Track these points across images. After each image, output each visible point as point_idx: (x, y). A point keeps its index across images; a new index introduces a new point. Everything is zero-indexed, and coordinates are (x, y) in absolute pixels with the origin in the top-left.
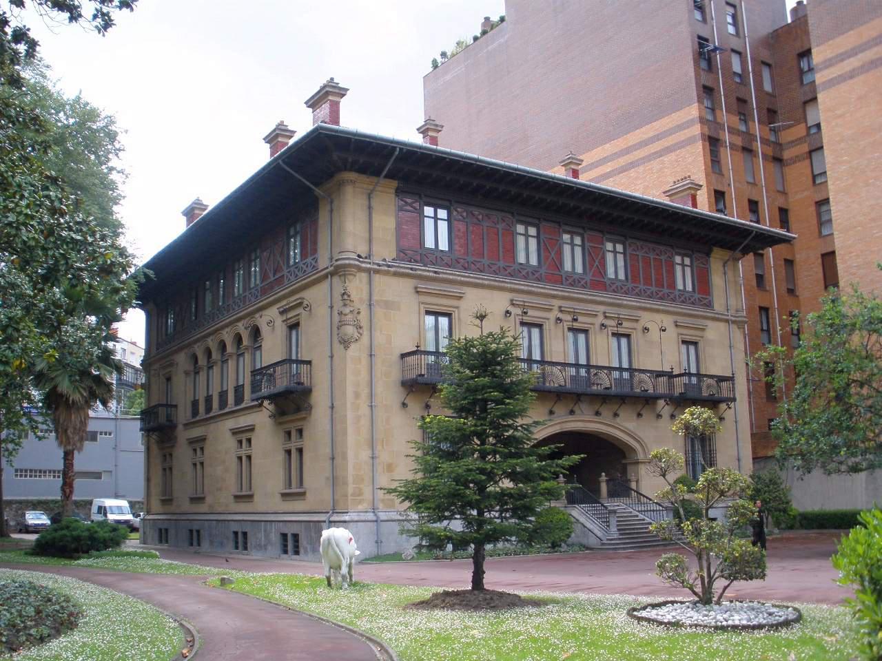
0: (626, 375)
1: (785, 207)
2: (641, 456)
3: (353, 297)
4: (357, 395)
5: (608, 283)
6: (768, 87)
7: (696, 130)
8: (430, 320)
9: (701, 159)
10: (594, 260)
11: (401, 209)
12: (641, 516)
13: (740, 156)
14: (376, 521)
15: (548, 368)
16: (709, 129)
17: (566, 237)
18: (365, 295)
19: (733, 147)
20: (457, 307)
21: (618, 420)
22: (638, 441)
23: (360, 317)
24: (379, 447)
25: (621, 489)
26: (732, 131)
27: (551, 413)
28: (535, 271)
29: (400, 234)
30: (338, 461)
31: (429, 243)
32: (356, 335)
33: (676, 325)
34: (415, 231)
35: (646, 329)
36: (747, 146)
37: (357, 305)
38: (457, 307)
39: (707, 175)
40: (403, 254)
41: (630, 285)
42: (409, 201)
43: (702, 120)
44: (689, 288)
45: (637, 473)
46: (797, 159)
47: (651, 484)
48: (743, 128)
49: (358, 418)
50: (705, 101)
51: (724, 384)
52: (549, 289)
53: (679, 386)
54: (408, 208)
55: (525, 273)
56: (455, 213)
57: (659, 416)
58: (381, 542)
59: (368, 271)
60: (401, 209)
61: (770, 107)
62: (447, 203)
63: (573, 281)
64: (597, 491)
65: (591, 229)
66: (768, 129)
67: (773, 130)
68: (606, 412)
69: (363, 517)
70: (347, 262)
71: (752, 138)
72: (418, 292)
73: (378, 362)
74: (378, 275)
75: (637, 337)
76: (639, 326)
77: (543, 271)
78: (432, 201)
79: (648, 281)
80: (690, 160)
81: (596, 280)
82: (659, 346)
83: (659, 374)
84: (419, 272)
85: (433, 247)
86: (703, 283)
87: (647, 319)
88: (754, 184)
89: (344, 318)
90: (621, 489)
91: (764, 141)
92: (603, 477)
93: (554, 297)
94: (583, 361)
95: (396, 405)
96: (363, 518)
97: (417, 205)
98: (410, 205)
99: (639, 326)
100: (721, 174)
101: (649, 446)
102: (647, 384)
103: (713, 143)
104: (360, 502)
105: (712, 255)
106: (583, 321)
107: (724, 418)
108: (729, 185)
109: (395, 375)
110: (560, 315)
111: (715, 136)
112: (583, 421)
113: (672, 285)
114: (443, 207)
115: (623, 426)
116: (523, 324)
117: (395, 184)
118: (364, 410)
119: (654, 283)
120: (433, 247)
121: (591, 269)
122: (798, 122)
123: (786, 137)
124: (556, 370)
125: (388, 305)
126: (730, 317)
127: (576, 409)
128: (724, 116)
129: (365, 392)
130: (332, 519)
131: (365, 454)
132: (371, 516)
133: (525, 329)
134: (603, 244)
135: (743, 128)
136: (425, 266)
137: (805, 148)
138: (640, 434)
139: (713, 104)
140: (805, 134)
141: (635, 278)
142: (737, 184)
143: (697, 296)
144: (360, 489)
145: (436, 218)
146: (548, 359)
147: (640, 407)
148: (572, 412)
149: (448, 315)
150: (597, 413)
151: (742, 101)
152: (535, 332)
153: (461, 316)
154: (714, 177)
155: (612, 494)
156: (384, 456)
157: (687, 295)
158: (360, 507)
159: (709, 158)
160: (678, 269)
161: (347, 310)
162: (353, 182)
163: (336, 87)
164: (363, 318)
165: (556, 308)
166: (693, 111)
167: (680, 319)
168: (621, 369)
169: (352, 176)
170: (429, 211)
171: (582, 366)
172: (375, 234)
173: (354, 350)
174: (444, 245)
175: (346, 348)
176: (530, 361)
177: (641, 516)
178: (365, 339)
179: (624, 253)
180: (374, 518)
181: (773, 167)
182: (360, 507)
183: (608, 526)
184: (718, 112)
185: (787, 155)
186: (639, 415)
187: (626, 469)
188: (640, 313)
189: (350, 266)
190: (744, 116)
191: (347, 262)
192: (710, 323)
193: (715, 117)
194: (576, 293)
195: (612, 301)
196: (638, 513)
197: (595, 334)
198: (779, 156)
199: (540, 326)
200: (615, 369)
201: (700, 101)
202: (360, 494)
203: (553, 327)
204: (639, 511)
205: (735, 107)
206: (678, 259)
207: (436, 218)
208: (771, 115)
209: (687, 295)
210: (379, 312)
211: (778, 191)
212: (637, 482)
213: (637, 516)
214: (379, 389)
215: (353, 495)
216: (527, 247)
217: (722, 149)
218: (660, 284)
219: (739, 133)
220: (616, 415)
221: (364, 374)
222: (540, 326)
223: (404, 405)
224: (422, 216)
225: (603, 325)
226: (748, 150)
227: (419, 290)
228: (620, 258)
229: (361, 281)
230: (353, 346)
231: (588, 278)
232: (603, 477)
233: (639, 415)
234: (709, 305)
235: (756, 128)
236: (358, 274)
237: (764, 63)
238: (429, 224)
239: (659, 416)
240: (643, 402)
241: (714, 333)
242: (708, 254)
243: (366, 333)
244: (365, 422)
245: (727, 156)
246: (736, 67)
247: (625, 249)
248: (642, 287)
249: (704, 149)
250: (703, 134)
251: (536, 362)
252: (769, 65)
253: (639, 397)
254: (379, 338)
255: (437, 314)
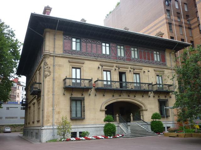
0: (109, 83)
1: (192, 40)
2: (144, 108)
3: (48, 63)
4: (48, 92)
5: (132, 59)
6: (186, 10)
7: (165, 21)
8: (74, 70)
9: (166, 29)
10: (128, 53)
11: (65, 39)
12: (142, 126)
13: (178, 28)
14: (53, 129)
15: (142, 85)
16: (168, 21)
17: (132, 49)
18: (52, 63)
19: (186, 27)
20: (82, 66)
21: (136, 98)
22: (142, 104)
23: (50, 69)
24: (55, 107)
25: (138, 118)
26: (175, 21)
27: (113, 96)
28: (137, 59)
29: (64, 46)
30: (43, 111)
31: (104, 52)
32: (49, 74)
33: (155, 71)
34: (69, 45)
35: (144, 72)
36: (180, 25)
37: (49, 66)
38: (82, 66)
39: (168, 33)
40: (65, 51)
41: (139, 60)
42: (67, 37)
43: (166, 18)
44: (159, 60)
45: (143, 114)
46: (195, 27)
47: (147, 116)
48: (179, 20)
49: (49, 98)
50: (167, 14)
51: (150, 86)
52: (128, 62)
53: (155, 88)
54: (67, 39)
55: (157, 63)
56: (82, 40)
57: (149, 97)
58: (53, 135)
59: (53, 56)
60: (65, 39)
61: (187, 15)
62: (109, 42)
63: (120, 58)
64: (130, 119)
65: (126, 44)
66: (186, 20)
67: (188, 20)
68: (132, 96)
69: (49, 128)
70: (46, 53)
71: (182, 23)
72: (69, 62)
73: (56, 82)
74: (56, 58)
75: (141, 74)
76: (142, 71)
77: (125, 58)
78: (104, 42)
79: (145, 58)
80: (164, 29)
81: (128, 58)
82: (149, 76)
83: (149, 84)
84: (118, 62)
85: (75, 50)
86: (163, 59)
87: (145, 69)
88: (183, 35)
89: (45, 69)
90: (138, 118)
91: (185, 23)
92: (132, 115)
93: (129, 65)
94: (161, 83)
95: (62, 94)
96: (48, 128)
97: (70, 38)
98: (68, 38)
99: (142, 71)
100: (173, 32)
101: (146, 105)
102: (145, 87)
103: (170, 24)
104: (48, 123)
105: (166, 51)
106: (136, 71)
107: (171, 97)
108: (175, 35)
109: (62, 85)
110: (116, 68)
111: (170, 22)
112: (124, 98)
113: (153, 59)
114: (108, 43)
115: (137, 100)
116: (134, 73)
117: (62, 32)
118: (51, 95)
119: (147, 59)
120: (75, 50)
121: (126, 54)
122: (195, 18)
123: (192, 22)
124: (143, 85)
125: (60, 66)
126: (172, 68)
127: (130, 95)
128: (173, 17)
129: (51, 90)
130: (41, 128)
131: (51, 109)
132: (52, 127)
133: (135, 75)
134: (130, 48)
135: (179, 20)
136: (72, 55)
137: (197, 24)
138: (143, 102)
139: (170, 14)
140: (197, 20)
141: (141, 57)
142: (178, 35)
143: (161, 62)
144: (49, 119)
145: (106, 46)
146: (141, 82)
147: (143, 94)
148: (120, 96)
149: (80, 68)
150: (129, 96)
151: (178, 13)
152: (138, 76)
153: (84, 69)
154: (170, 33)
155: (134, 120)
156: (57, 109)
157: (158, 62)
158: (48, 125)
159: (169, 28)
160: (155, 55)
161: (46, 67)
162: (49, 32)
163: (49, 7)
164: (51, 70)
165: (115, 66)
166: (164, 16)
167: (155, 69)
168: (137, 83)
169: (48, 30)
170: (104, 44)
171: (161, 84)
172: (56, 46)
173: (47, 79)
174: (108, 53)
175: (46, 78)
176: (76, 79)
177: (142, 126)
178: (52, 75)
179: (137, 51)
180: (52, 128)
181: (189, 31)
182: (48, 125)
183: (127, 128)
184: (171, 16)
185: (192, 27)
186: (143, 96)
187: (140, 112)
188: (142, 67)
189: (46, 54)
190: (179, 17)
191: (46, 53)
192: (165, 70)
193: (170, 17)
194: (122, 62)
195: (133, 64)
196: (140, 126)
197: (128, 73)
198: (190, 27)
199: (139, 74)
200: (135, 83)
201: (166, 13)
202: (49, 121)
203: (114, 72)
204: (141, 125)
205: (185, 17)
206: (155, 52)
207: (106, 46)
208: (187, 16)
209: (158, 62)
210: (57, 68)
211: (190, 37)
212: (143, 116)
213: (140, 126)
214: (56, 89)
215: (46, 121)
216: (157, 57)
217: (173, 26)
218: (149, 59)
219: (178, 21)
220: (135, 96)
221: (51, 85)
222: (139, 74)
223: (64, 94)
224: (102, 46)
225: (130, 71)
226: (180, 26)
227: (162, 73)
228: (136, 52)
229: (51, 59)
230: (48, 77)
231: (125, 58)
232: (132, 115)
233: (143, 96)
234: (165, 65)
235: (183, 20)
236: (50, 57)
237: (185, 3)
238: (104, 48)
239: (149, 97)
240: (144, 93)
241: (166, 72)
242: (165, 51)
243: (52, 74)
244: (51, 100)
245: (174, 28)
246: (177, 7)
247: (137, 49)
248: (143, 60)
249: (167, 26)
250: (166, 22)
251: (109, 81)
252: (186, 4)
253: (143, 91)
254: (56, 75)
255: (76, 68)
